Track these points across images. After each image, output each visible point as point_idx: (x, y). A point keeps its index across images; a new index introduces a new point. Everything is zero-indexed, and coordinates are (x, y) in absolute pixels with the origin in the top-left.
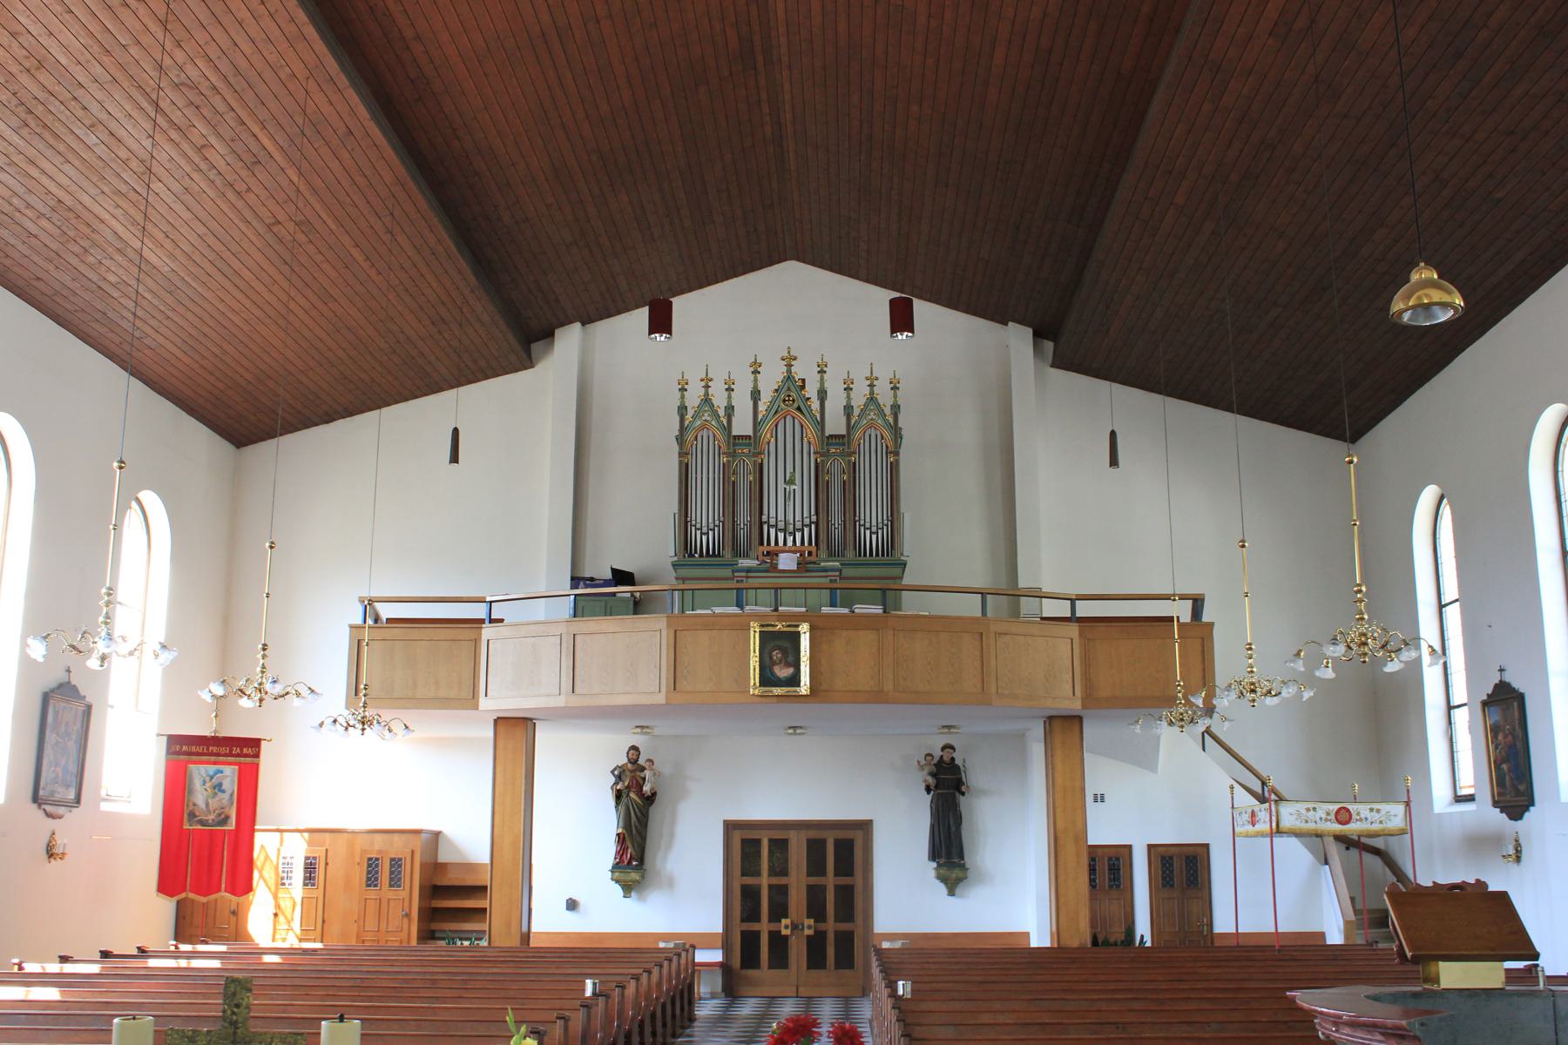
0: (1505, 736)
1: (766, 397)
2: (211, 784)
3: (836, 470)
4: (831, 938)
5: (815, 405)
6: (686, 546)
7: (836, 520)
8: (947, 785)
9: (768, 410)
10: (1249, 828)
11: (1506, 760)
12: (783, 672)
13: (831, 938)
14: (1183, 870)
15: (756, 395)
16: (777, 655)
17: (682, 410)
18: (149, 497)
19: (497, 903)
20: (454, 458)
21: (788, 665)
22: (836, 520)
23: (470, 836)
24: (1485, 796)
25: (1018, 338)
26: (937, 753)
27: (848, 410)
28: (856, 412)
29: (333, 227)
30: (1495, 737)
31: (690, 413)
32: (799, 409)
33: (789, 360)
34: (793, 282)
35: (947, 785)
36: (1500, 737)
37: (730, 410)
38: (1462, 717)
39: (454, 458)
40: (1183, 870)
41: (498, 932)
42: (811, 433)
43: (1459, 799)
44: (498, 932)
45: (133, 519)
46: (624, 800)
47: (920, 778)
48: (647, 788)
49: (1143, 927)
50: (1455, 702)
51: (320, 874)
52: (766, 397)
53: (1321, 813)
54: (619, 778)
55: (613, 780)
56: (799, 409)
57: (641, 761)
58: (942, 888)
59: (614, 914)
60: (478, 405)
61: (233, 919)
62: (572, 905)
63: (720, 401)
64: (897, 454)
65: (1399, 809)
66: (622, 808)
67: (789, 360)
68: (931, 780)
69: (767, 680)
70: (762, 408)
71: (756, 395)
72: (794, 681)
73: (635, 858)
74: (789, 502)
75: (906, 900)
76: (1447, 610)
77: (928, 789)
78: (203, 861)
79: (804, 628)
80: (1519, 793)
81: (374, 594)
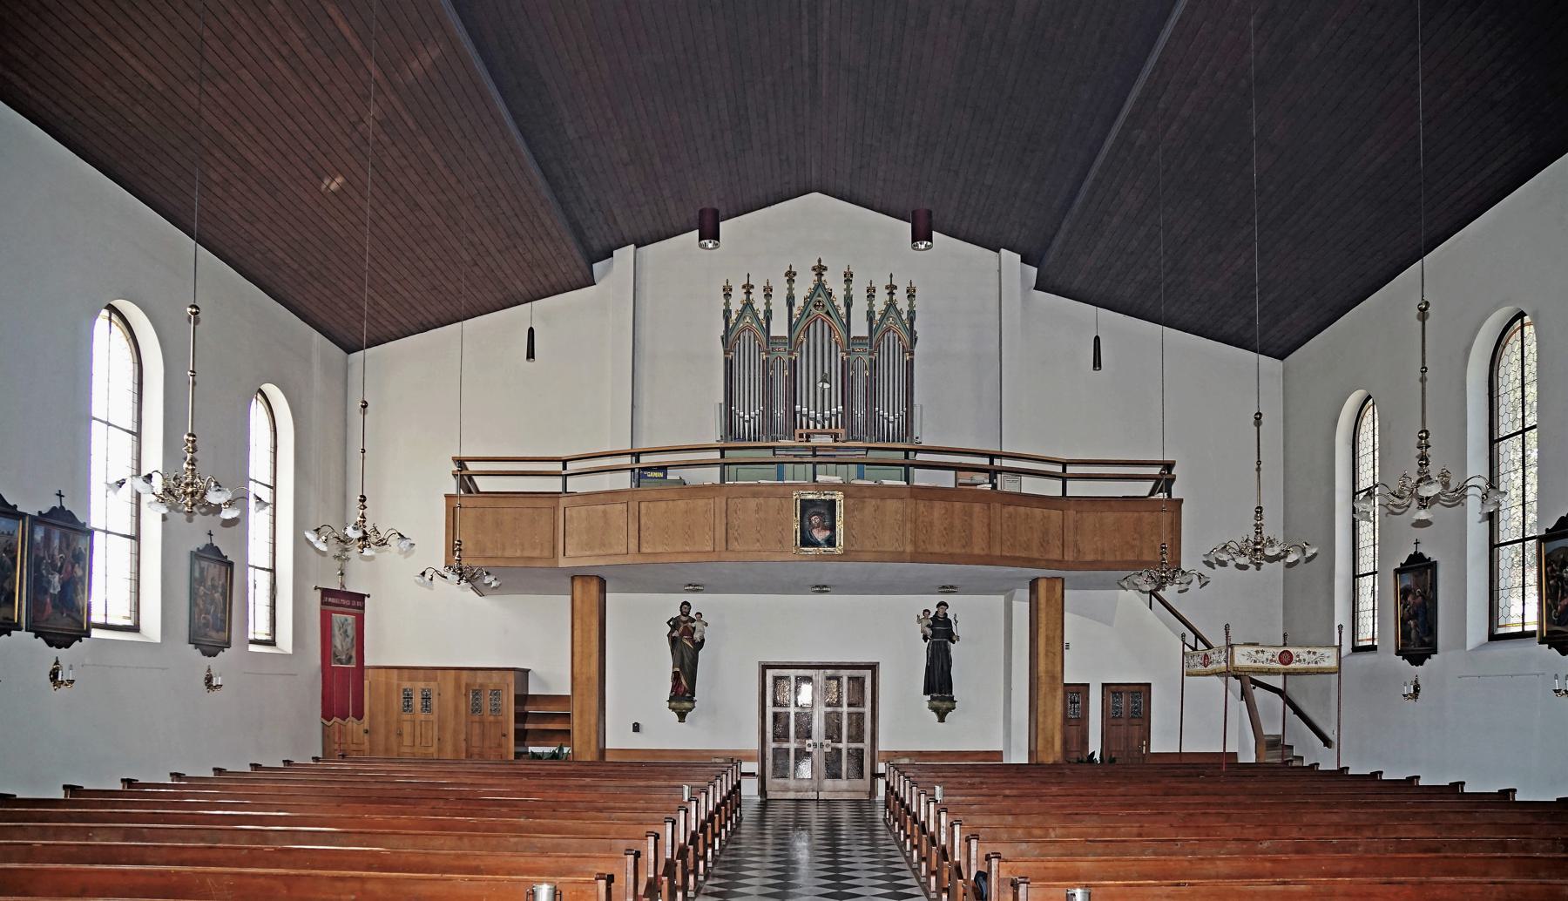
0: (1415, 598)
1: (799, 303)
2: (342, 620)
3: (859, 365)
4: (845, 716)
5: (843, 310)
6: (729, 429)
7: (859, 413)
8: (940, 632)
9: (802, 314)
10: (1200, 668)
11: (1414, 616)
12: (820, 535)
13: (845, 716)
14: (1130, 702)
15: (790, 302)
16: (815, 520)
17: (727, 314)
18: (271, 389)
19: (579, 726)
20: (531, 355)
21: (825, 528)
22: (859, 413)
23: (553, 674)
24: (1390, 642)
25: (1011, 258)
26: (933, 611)
27: (870, 316)
28: (878, 317)
29: (413, 127)
30: (1404, 598)
31: (734, 316)
32: (828, 313)
33: (820, 270)
34: (817, 210)
35: (940, 632)
36: (1410, 599)
37: (768, 314)
38: (1366, 584)
39: (531, 355)
40: (1130, 702)
41: (580, 747)
42: (839, 333)
43: (1356, 649)
44: (580, 747)
45: (258, 411)
46: (678, 645)
47: (917, 630)
48: (697, 636)
49: (1095, 746)
50: (1362, 570)
51: (434, 701)
52: (799, 303)
53: (1268, 655)
54: (674, 628)
55: (669, 629)
56: (828, 313)
57: (692, 614)
58: (934, 716)
59: (666, 734)
60: (552, 314)
61: (366, 737)
62: (636, 728)
63: (759, 305)
64: (912, 353)
65: (1333, 652)
66: (678, 655)
67: (820, 270)
68: (929, 632)
69: (807, 541)
70: (795, 311)
71: (790, 302)
72: (831, 542)
73: (683, 694)
74: (819, 401)
75: (903, 723)
76: (1502, 446)
77: (925, 638)
78: (343, 684)
79: (839, 497)
80: (1423, 644)
81: (464, 454)
